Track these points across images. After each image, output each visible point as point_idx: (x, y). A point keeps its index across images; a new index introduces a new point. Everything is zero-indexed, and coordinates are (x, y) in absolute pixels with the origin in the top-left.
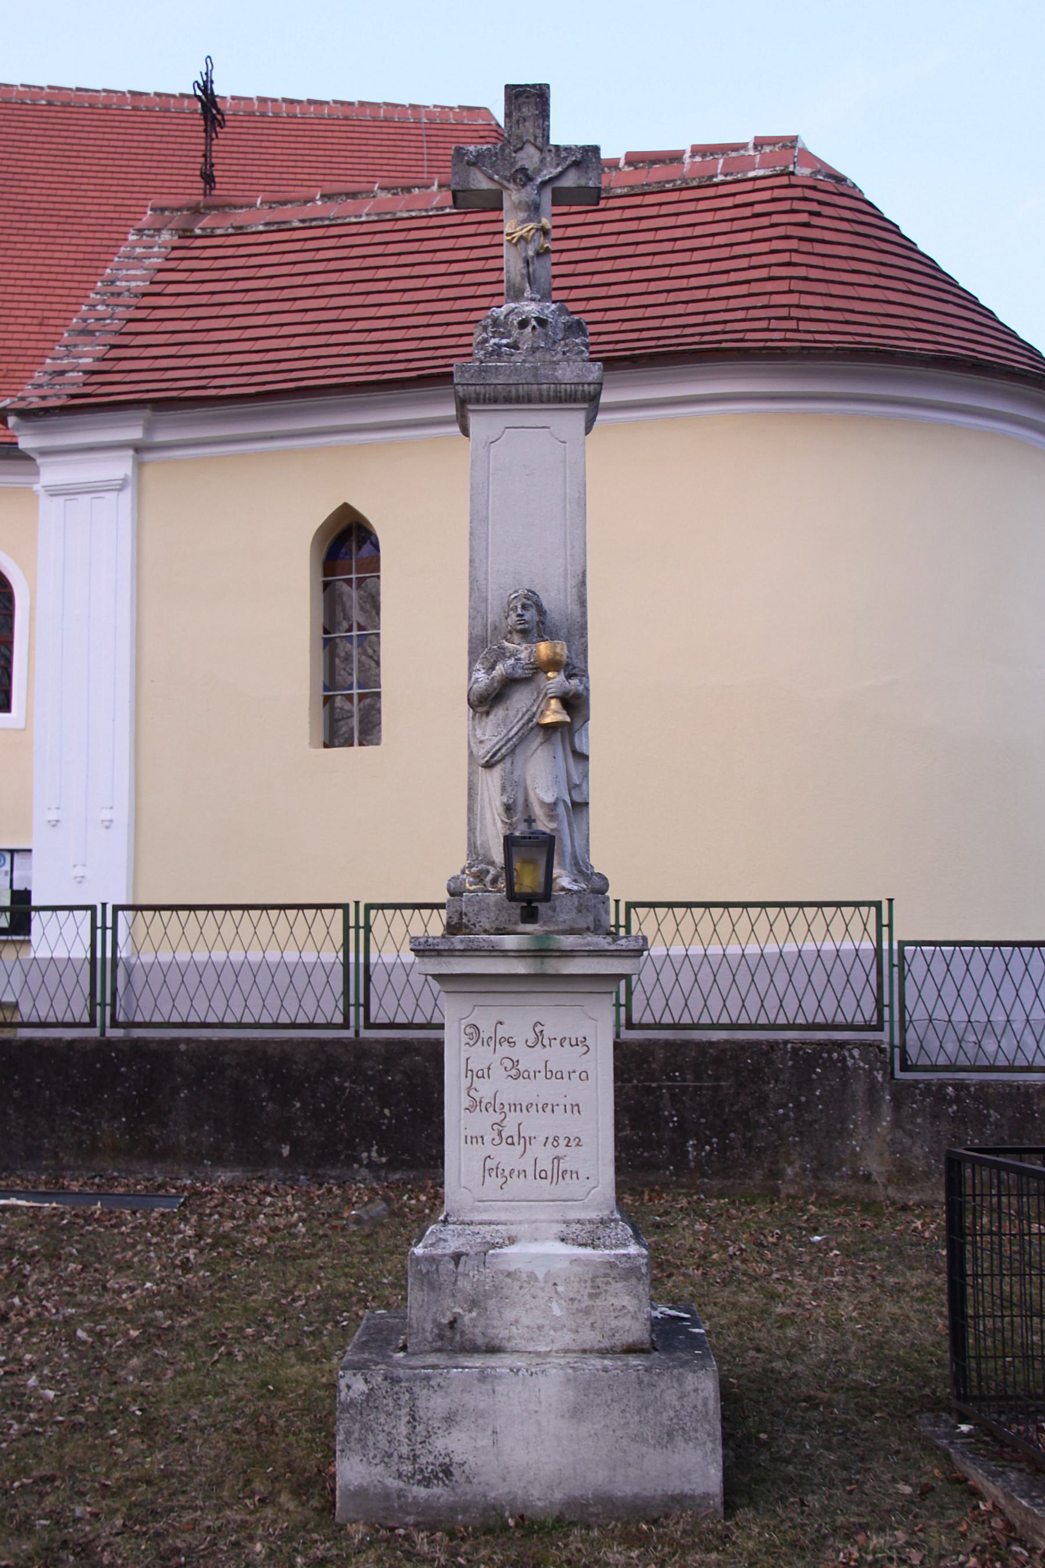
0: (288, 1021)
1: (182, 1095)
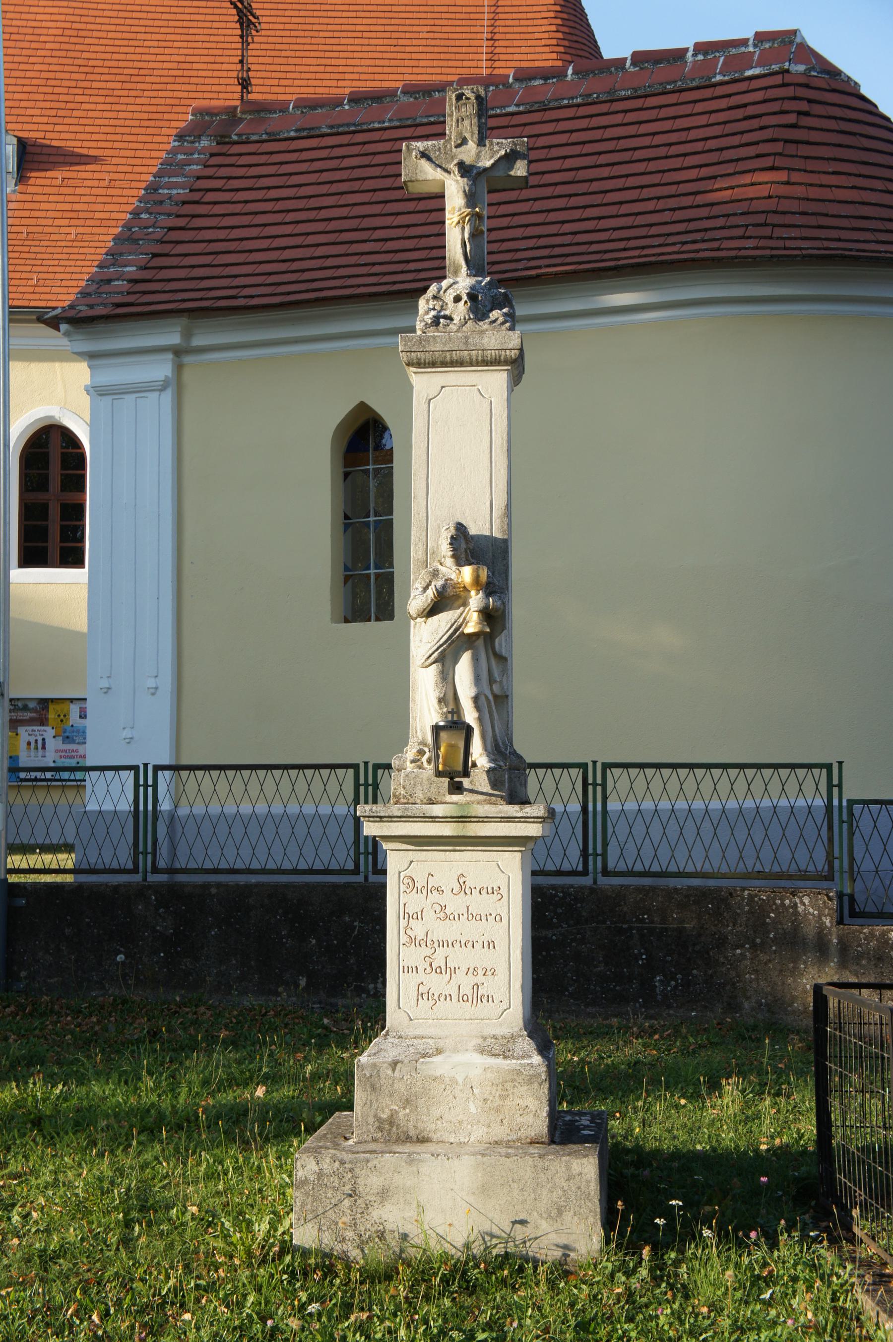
0: (306, 867)
1: (213, 933)
